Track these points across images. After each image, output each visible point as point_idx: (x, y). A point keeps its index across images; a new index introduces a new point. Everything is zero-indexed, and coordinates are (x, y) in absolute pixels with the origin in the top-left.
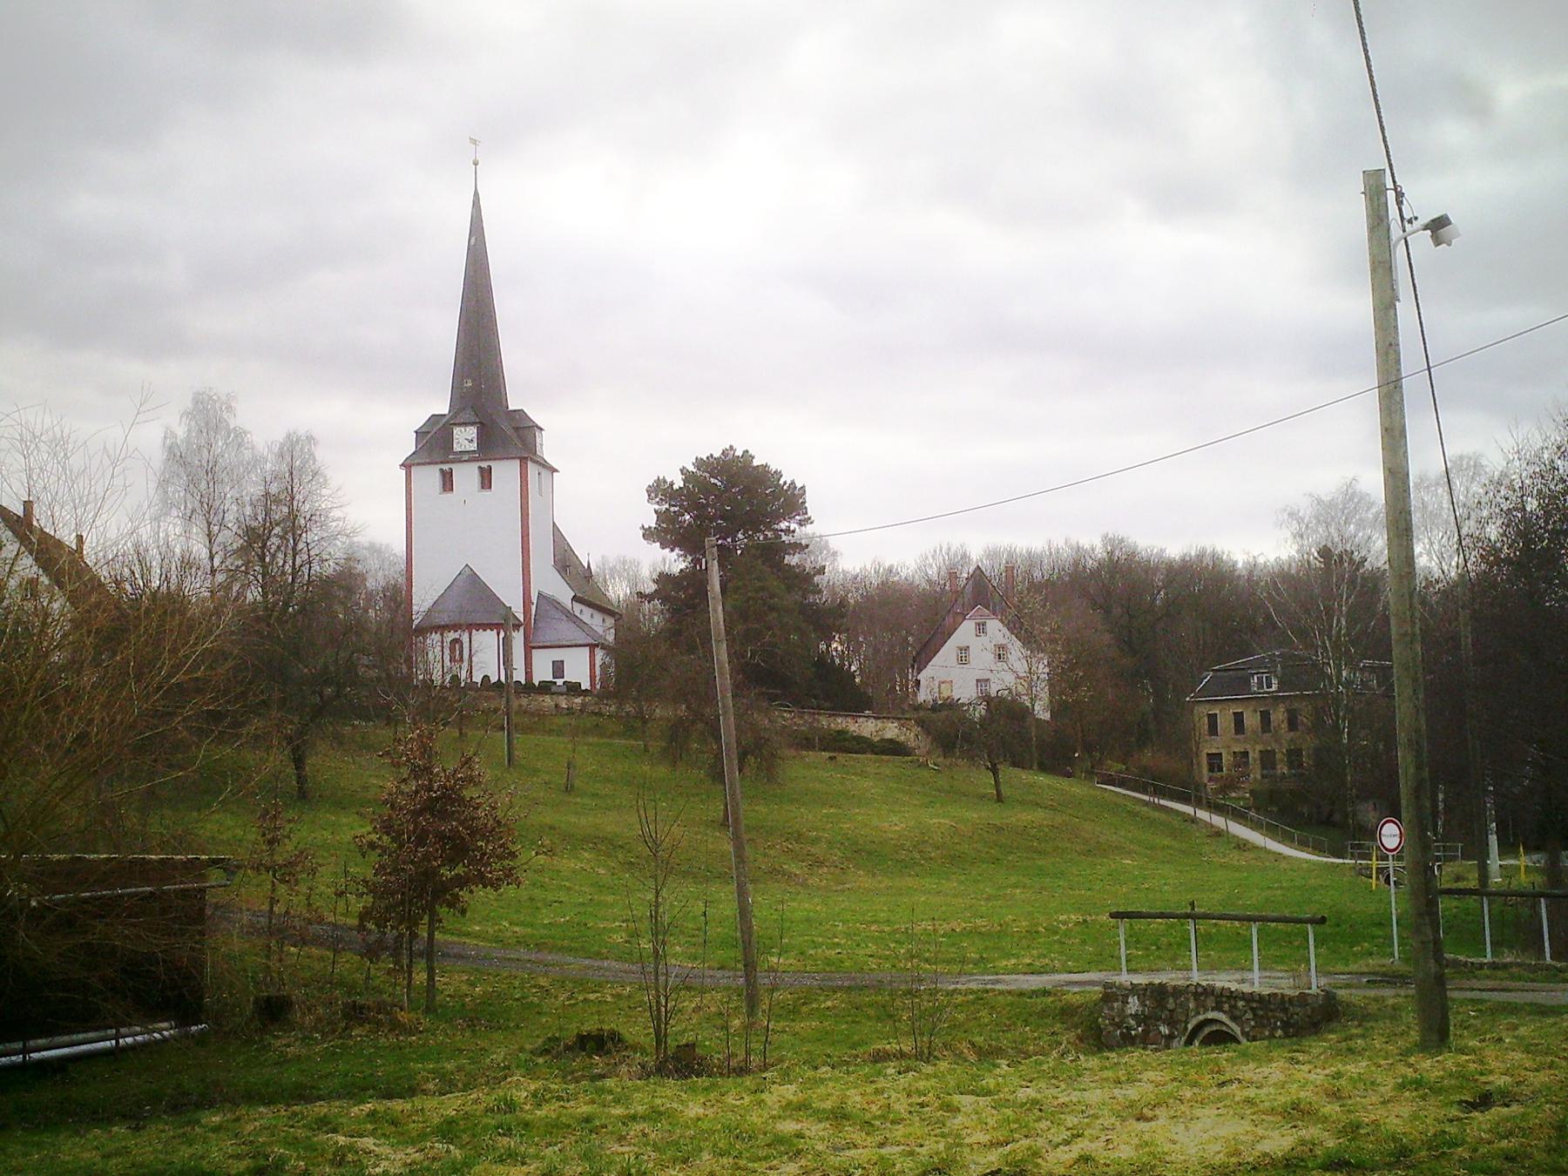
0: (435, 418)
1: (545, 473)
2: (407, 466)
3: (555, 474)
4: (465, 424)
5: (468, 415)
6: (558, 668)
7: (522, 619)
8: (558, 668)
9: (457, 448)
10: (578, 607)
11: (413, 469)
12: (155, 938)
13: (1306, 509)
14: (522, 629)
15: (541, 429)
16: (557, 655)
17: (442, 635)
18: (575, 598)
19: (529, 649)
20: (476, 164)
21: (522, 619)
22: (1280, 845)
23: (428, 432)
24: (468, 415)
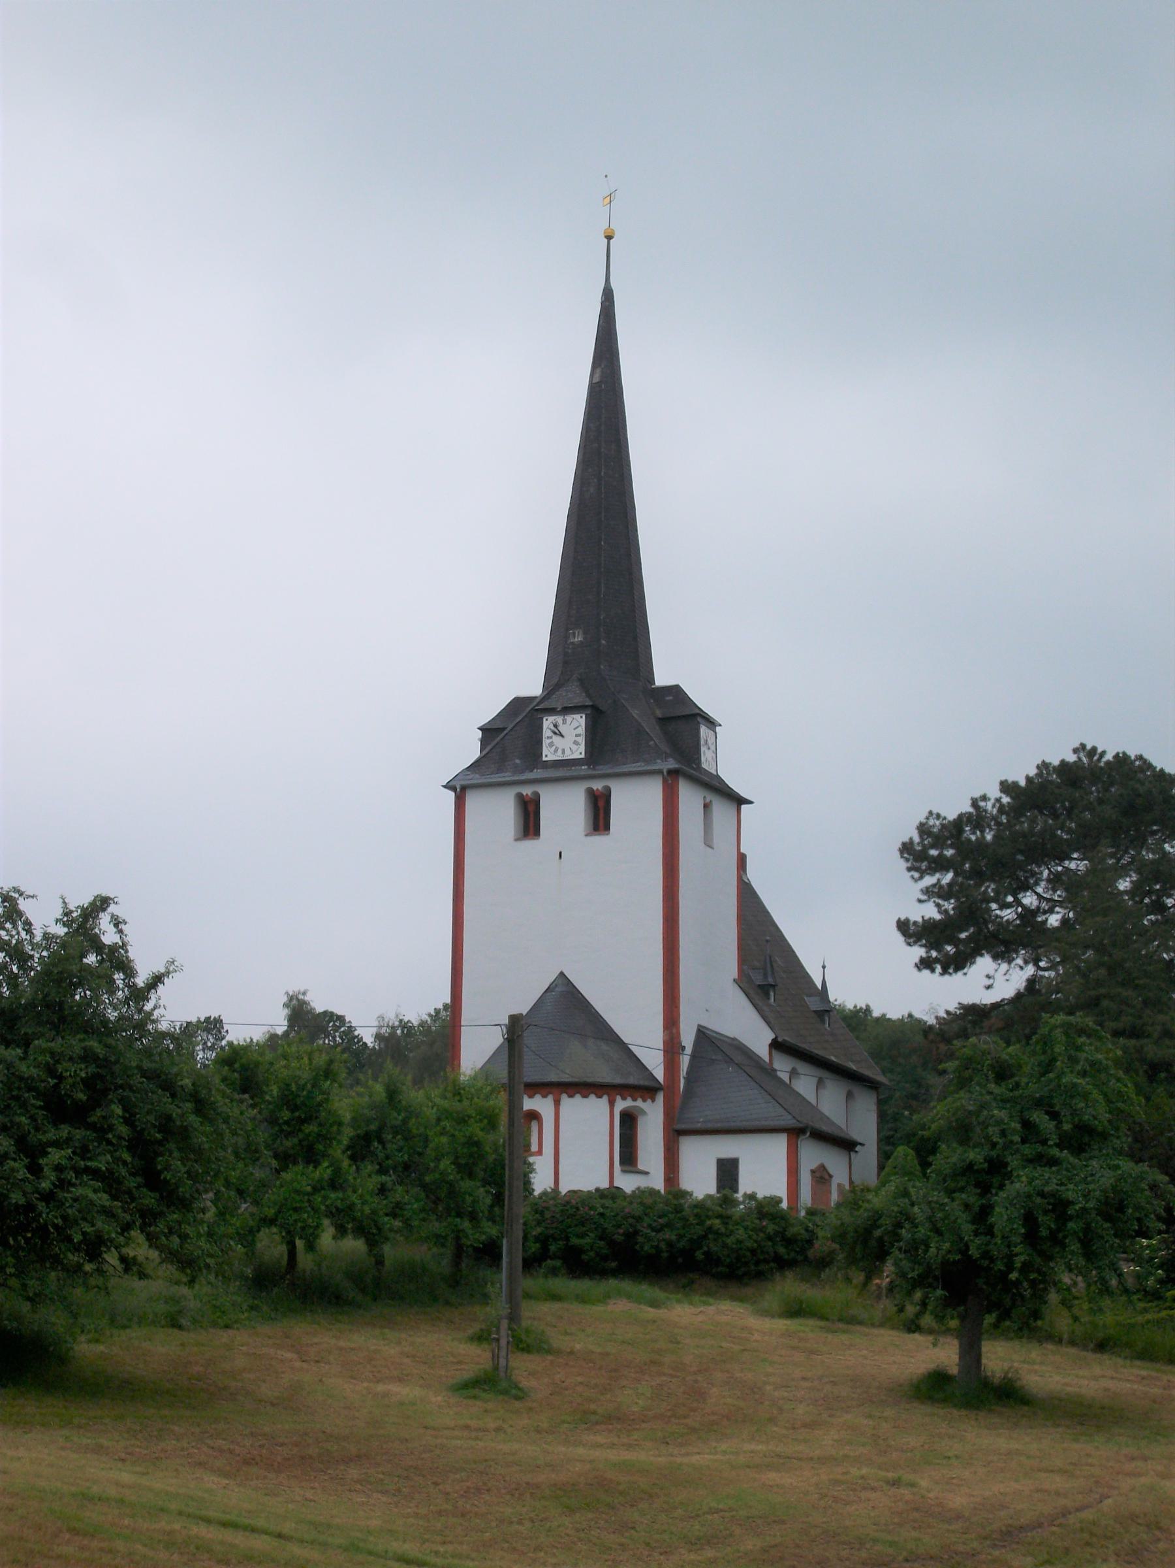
0: (518, 704)
1: (722, 811)
2: (460, 789)
3: (744, 808)
4: (567, 710)
5: (573, 693)
6: (728, 1171)
7: (659, 1074)
8: (728, 1171)
9: (548, 754)
10: (783, 1066)
11: (473, 801)
12: (1118, 1080)
13: (866, 1184)
14: (660, 1097)
15: (740, 801)
16: (727, 1147)
17: (557, 1103)
18: (776, 1045)
19: (675, 1134)
20: (609, 238)
21: (659, 1074)
22: (832, 1191)
23: (504, 729)
24: (573, 693)
